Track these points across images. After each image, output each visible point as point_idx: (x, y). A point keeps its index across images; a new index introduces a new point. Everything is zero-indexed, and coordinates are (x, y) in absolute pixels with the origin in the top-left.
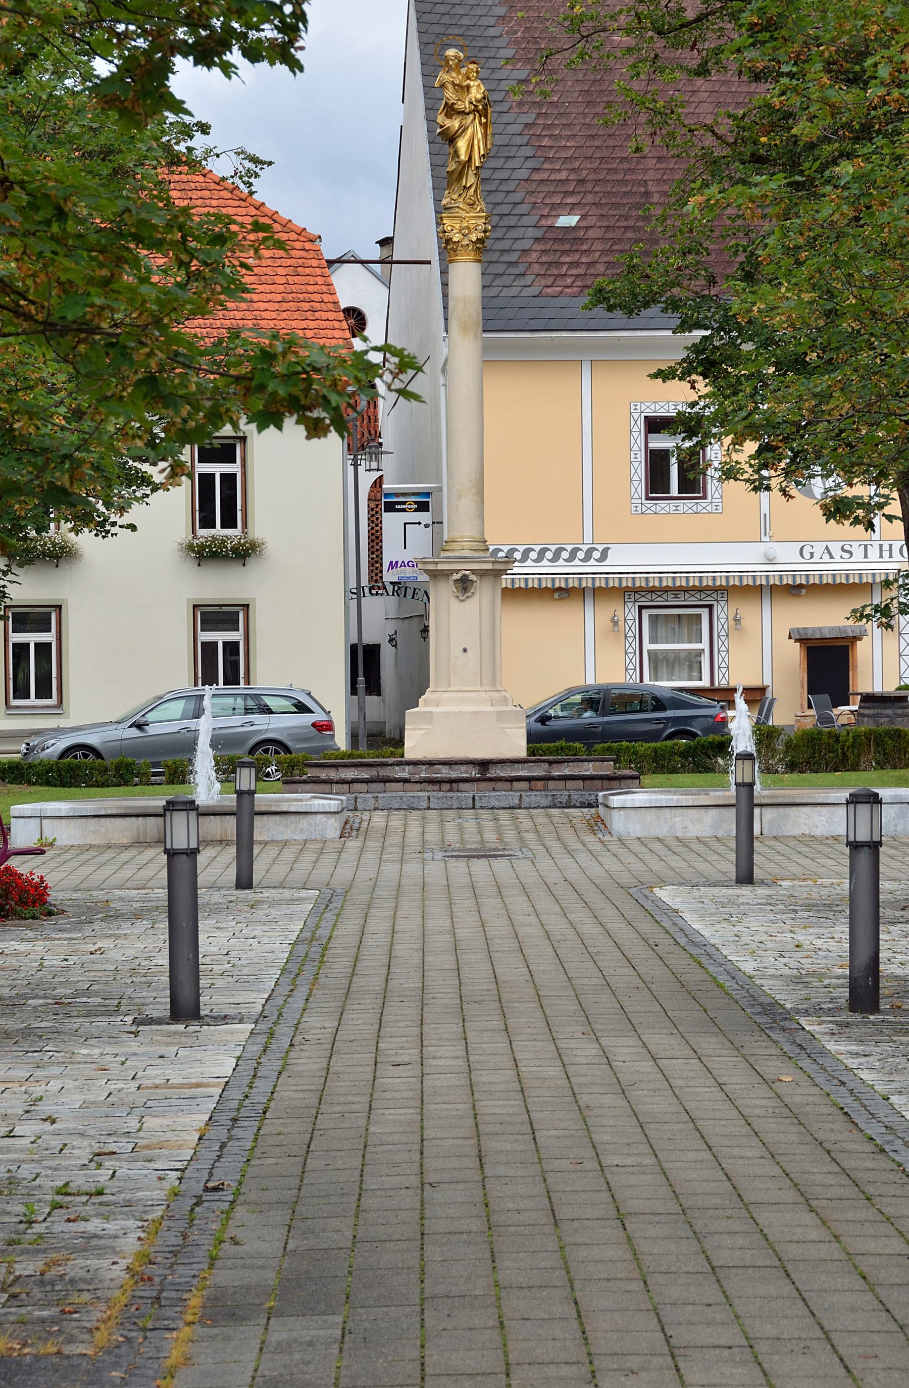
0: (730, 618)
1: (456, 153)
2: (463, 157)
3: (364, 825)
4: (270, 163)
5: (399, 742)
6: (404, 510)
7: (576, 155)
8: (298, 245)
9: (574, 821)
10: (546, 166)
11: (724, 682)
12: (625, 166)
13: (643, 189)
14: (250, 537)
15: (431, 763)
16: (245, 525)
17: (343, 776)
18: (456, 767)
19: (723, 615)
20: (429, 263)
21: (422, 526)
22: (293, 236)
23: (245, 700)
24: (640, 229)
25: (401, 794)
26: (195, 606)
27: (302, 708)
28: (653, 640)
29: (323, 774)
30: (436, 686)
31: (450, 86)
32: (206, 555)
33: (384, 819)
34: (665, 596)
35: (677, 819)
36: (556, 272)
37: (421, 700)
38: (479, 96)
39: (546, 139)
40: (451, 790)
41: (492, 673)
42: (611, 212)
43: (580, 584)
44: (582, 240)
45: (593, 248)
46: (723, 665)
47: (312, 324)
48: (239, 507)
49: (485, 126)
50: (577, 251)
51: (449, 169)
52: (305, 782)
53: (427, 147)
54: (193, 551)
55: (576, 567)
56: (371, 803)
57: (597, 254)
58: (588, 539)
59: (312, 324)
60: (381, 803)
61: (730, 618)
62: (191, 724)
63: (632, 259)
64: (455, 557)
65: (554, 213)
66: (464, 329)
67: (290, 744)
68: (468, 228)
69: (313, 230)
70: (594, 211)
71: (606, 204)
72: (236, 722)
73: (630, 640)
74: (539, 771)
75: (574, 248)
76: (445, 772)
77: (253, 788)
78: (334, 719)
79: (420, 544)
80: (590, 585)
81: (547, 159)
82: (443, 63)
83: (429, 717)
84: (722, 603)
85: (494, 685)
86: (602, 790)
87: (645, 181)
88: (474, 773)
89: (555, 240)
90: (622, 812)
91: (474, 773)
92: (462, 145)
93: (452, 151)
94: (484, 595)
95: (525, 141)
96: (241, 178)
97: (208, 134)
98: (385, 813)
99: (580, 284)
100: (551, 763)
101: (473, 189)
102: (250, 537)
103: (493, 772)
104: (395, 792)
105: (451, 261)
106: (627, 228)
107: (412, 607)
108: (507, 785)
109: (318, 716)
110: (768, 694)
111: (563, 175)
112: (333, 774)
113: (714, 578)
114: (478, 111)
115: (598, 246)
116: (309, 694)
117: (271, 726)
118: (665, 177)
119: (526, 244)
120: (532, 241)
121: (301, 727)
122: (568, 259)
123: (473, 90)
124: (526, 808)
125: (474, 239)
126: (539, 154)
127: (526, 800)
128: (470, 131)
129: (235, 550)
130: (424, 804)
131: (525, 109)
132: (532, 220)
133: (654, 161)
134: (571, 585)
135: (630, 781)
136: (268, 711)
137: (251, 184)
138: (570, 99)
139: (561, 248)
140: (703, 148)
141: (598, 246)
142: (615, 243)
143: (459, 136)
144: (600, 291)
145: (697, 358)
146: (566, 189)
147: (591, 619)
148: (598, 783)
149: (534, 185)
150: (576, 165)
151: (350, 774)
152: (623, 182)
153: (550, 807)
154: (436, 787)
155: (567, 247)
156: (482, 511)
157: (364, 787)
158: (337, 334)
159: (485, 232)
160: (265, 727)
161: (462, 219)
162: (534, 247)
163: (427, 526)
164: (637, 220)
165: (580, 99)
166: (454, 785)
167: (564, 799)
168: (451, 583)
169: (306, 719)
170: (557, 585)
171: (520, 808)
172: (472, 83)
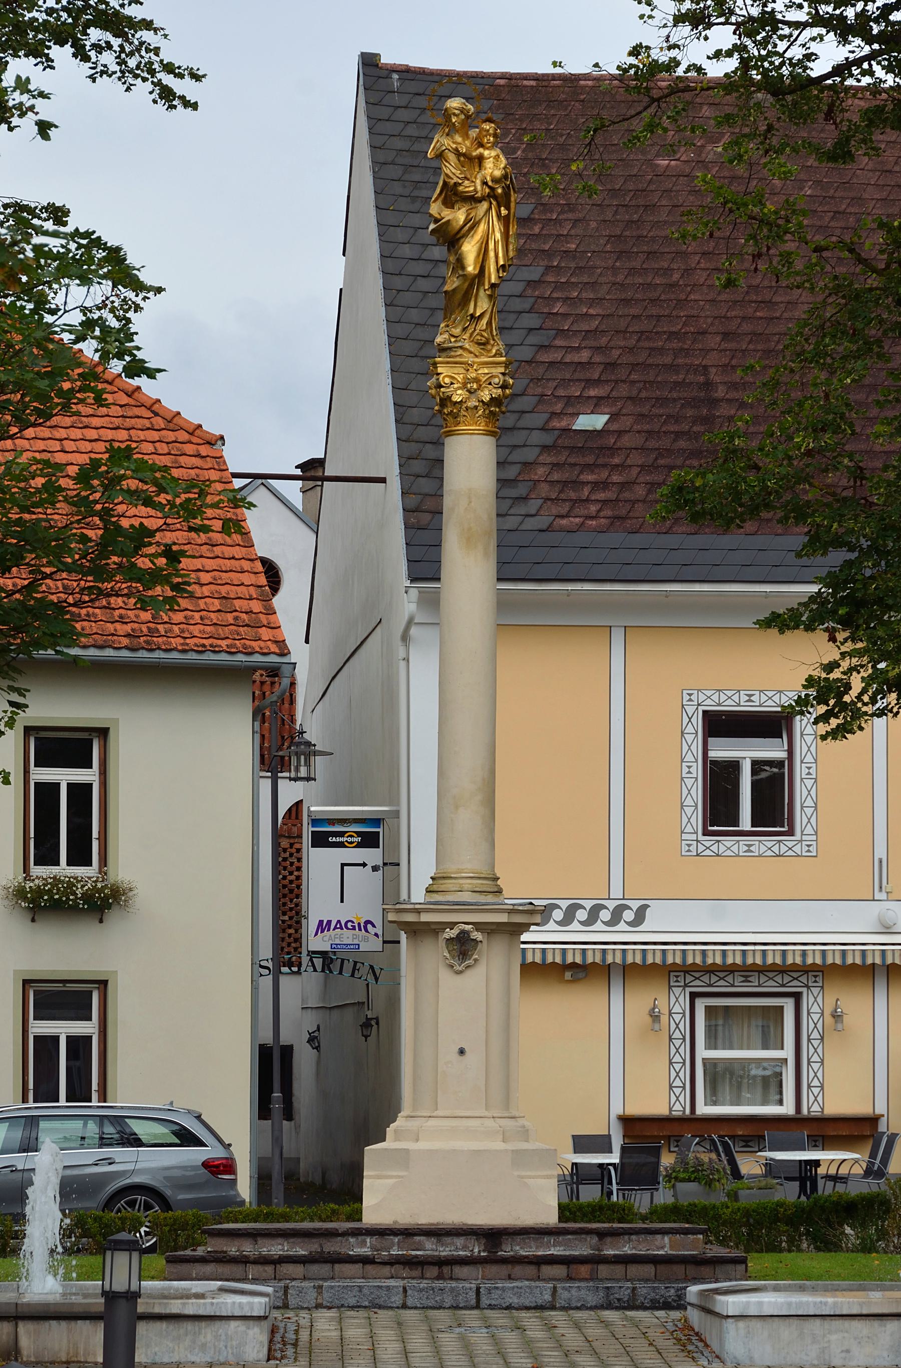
0: (827, 1013)
1: (460, 263)
2: (471, 268)
3: (304, 1335)
4: (159, 290)
5: (351, 1193)
6: (341, 845)
7: (603, 327)
8: (189, 449)
9: (651, 1334)
10: (558, 342)
11: (816, 1108)
12: (675, 344)
13: (702, 379)
14: (112, 878)
15: (407, 1233)
16: (104, 861)
17: (264, 1251)
18: (448, 1240)
19: (815, 1008)
20: (383, 480)
21: (369, 868)
22: (183, 436)
23: (101, 1125)
24: (697, 436)
25: (360, 1282)
26: (26, 983)
27: (186, 1138)
28: (712, 1043)
29: (232, 1248)
30: (415, 1108)
31: (452, 157)
32: (43, 905)
33: (334, 1326)
34: (730, 979)
35: (834, 1337)
36: (573, 495)
37: (390, 1131)
38: (498, 173)
39: (559, 304)
40: (440, 1277)
41: (503, 1092)
42: (655, 411)
43: (604, 959)
44: (613, 450)
45: (629, 462)
46: (816, 1083)
47: (210, 564)
48: (95, 834)
49: (505, 221)
50: (604, 466)
51: (447, 288)
52: (202, 1260)
53: (381, 312)
54: (25, 899)
55: (599, 933)
56: (311, 1297)
57: (635, 471)
58: (616, 892)
59: (210, 564)
60: (326, 1296)
61: (827, 1013)
62: (19, 1160)
63: (732, 439)
64: (448, 903)
65: (570, 410)
66: (469, 540)
67: (168, 1192)
68: (476, 380)
69: (211, 428)
70: (630, 408)
71: (648, 399)
72: (87, 1158)
73: (677, 1043)
74: (582, 1248)
75: (600, 461)
76: (430, 1248)
77: (134, 1287)
78: (237, 1156)
79: (363, 899)
80: (618, 960)
81: (560, 332)
82: (440, 120)
83: (403, 1158)
84: (815, 991)
85: (507, 1107)
86: (696, 1280)
87: (705, 367)
88: (477, 1249)
89: (572, 449)
90: (741, 1324)
91: (477, 1249)
92: (470, 249)
93: (452, 259)
94: (493, 965)
95: (527, 306)
96: (112, 311)
97: (69, 211)
98: (333, 1313)
99: (609, 513)
100: (602, 1235)
101: (485, 321)
102: (112, 878)
103: (508, 1249)
104: (349, 1282)
105: (449, 434)
106: (678, 435)
107: (350, 990)
108: (531, 1270)
109: (211, 1151)
110: (882, 1127)
111: (584, 356)
112: (248, 1248)
113: (804, 953)
114: (496, 197)
115: (636, 459)
116: (199, 1117)
117: (139, 1166)
118: (734, 362)
119: (530, 455)
120: (537, 450)
121: (184, 1168)
122: (591, 478)
123: (489, 164)
124: (563, 1308)
125: (487, 398)
126: (549, 324)
127: (563, 1296)
128: (482, 227)
129: (88, 897)
130: (397, 1300)
131: (528, 260)
132: (539, 419)
133: (718, 339)
134: (590, 960)
135: (730, 1267)
136: (136, 1142)
137: (129, 321)
138: (593, 247)
139: (581, 460)
140: (836, 278)
141: (636, 459)
142: (660, 455)
143: (465, 236)
144: (680, 489)
145: (833, 595)
146: (588, 375)
147: (619, 1011)
148: (679, 1269)
149: (541, 370)
150: (604, 341)
151: (276, 1248)
152: (673, 368)
153: (602, 1307)
154: (417, 1273)
155: (590, 459)
156: (492, 831)
157: (297, 1270)
158: (247, 579)
159: (504, 387)
160: (130, 1167)
161: (468, 366)
162: (541, 459)
163: (375, 869)
164: (694, 423)
165: (608, 248)
166: (446, 1270)
167: (625, 1294)
168: (442, 943)
169: (194, 1156)
170: (570, 960)
171: (553, 1308)
172: (487, 153)
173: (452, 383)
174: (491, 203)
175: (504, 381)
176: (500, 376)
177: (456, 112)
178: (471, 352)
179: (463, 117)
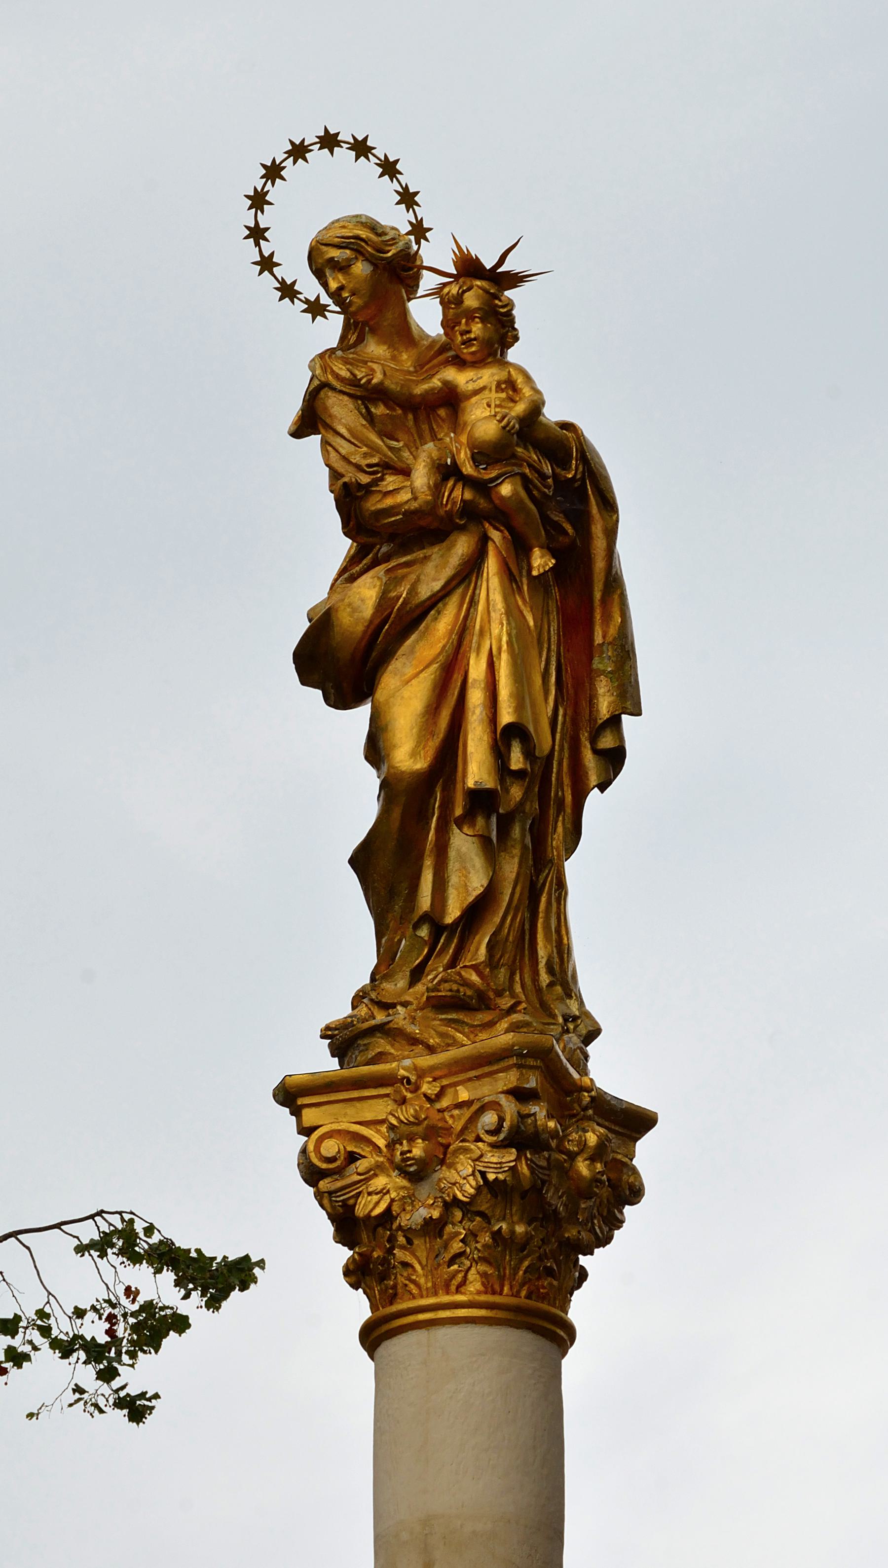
173: (352, 1157)
174: (484, 540)
175: (522, 1117)
176: (503, 1100)
177: (335, 253)
178: (414, 1041)
179: (361, 268)
